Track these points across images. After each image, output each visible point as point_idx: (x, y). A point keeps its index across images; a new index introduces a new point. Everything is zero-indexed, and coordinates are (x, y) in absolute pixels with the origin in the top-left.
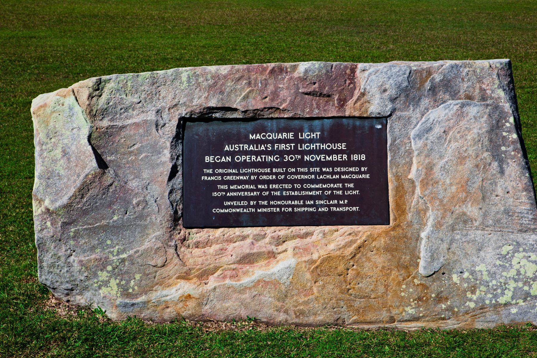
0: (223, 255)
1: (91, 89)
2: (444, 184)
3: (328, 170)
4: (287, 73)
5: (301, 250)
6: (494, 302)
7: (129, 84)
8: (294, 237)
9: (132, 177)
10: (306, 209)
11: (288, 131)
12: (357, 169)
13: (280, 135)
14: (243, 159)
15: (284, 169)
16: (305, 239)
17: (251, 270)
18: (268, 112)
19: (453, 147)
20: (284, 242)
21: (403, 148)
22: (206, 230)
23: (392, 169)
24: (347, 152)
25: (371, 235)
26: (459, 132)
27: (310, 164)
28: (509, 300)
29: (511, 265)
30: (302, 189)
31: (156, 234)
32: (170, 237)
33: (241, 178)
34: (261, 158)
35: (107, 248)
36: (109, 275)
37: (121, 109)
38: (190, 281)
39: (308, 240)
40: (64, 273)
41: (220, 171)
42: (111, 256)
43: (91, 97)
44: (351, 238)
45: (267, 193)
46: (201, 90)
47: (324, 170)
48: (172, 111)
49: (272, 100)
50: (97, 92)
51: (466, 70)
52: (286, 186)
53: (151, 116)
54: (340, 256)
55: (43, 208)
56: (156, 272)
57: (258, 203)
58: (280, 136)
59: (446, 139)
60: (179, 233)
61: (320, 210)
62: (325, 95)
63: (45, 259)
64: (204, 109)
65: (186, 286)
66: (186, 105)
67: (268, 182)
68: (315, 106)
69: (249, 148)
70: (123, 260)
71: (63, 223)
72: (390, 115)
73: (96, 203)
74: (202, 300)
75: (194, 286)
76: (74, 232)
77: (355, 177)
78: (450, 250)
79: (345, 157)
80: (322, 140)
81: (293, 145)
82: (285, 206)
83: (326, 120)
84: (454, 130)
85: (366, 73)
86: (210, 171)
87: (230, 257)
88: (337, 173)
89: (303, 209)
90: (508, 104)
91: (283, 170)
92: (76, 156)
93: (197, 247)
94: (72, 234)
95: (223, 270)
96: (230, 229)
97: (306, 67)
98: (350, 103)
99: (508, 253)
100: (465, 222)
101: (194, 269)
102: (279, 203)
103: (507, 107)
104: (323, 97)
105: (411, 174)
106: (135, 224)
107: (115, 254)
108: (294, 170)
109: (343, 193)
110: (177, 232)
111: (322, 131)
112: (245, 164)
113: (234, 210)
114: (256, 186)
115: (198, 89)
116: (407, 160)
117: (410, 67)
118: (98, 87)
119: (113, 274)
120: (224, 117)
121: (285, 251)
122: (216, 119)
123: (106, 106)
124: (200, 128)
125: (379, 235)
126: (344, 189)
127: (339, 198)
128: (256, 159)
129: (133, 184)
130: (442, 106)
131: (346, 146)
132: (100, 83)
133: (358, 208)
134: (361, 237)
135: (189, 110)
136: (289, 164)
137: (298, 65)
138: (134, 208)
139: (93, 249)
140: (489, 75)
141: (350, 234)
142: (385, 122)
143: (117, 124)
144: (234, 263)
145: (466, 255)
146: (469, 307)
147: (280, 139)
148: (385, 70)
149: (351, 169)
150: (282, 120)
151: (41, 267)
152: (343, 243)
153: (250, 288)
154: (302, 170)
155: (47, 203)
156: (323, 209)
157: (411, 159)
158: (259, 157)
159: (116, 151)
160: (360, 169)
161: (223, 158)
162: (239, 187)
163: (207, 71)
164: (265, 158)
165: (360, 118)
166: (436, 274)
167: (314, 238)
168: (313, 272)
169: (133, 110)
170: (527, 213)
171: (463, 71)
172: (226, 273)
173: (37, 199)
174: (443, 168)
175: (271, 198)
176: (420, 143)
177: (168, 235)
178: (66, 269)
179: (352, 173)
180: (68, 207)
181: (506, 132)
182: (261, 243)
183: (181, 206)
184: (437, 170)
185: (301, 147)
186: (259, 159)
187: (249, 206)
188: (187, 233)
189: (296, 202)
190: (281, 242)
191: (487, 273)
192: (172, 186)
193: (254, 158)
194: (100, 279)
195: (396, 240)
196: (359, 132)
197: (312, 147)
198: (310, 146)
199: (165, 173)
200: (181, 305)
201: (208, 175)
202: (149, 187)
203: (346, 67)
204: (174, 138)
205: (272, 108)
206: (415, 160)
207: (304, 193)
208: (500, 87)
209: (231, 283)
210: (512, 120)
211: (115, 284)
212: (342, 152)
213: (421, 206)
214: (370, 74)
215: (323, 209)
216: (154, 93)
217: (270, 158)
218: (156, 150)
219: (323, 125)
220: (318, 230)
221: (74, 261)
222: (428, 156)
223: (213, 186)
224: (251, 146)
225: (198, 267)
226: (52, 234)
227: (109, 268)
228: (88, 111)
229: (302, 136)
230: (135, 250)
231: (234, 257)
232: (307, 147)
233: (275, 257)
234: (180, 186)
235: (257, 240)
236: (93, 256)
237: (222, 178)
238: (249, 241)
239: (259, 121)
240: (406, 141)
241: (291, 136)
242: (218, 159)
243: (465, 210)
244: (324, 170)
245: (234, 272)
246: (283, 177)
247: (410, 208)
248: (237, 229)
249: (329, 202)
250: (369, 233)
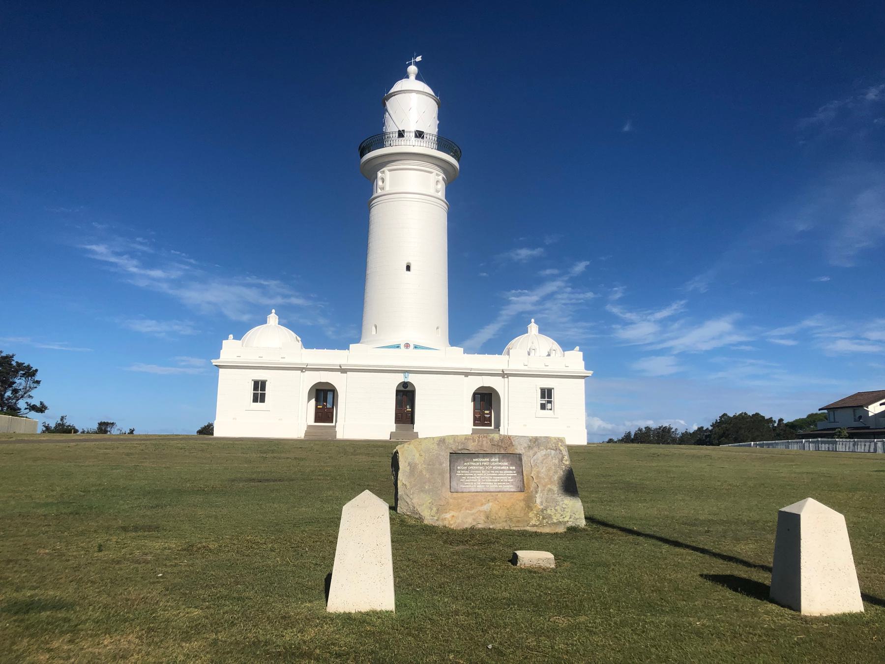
12: (512, 472)
77: (511, 475)
212: (506, 466)
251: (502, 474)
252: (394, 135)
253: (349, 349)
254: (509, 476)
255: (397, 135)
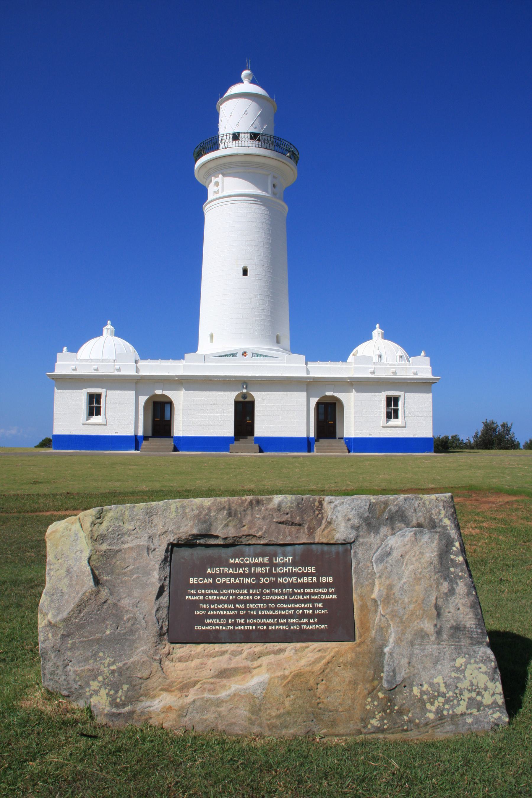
0: (203, 669)
1: (94, 517)
2: (403, 602)
3: (299, 591)
4: (263, 504)
5: (274, 666)
6: (451, 712)
7: (127, 513)
8: (269, 653)
9: (125, 595)
10: (279, 627)
11: (263, 556)
12: (325, 590)
13: (256, 559)
14: (223, 581)
15: (260, 590)
16: (278, 655)
17: (228, 684)
18: (246, 539)
19: (410, 569)
20: (259, 657)
21: (366, 571)
22: (188, 645)
23: (356, 590)
24: (317, 574)
25: (338, 651)
26: (414, 556)
27: (283, 586)
28: (464, 710)
29: (464, 676)
30: (276, 609)
31: (142, 648)
32: (156, 651)
33: (221, 598)
34: (240, 580)
35: (100, 660)
36: (100, 685)
37: (118, 535)
38: (172, 693)
39: (282, 656)
40: (62, 681)
41: (203, 591)
42: (102, 667)
43: (93, 524)
44: (320, 654)
45: (245, 612)
46: (187, 519)
47: (296, 591)
48: (162, 537)
49: (250, 528)
50: (99, 520)
51: (417, 503)
52: (261, 606)
53: (143, 542)
54: (310, 672)
55: (46, 621)
56: (142, 683)
57: (235, 621)
58: (256, 561)
59: (403, 563)
60: (164, 648)
61: (292, 628)
62: (296, 524)
63: (47, 667)
64: (189, 536)
65: (168, 698)
66: (174, 532)
67: (245, 602)
68: (287, 533)
69: (228, 571)
70: (113, 672)
71: (62, 635)
72: (354, 541)
73: (91, 618)
74: (182, 712)
75: (175, 699)
76: (71, 644)
77: (324, 597)
78: (411, 664)
79: (315, 579)
80: (294, 564)
81: (268, 568)
82: (260, 624)
83: (297, 546)
84: (410, 553)
85: (332, 505)
86: (194, 591)
87: (209, 671)
88: (308, 594)
89: (277, 627)
90: (454, 531)
91: (259, 591)
92: (77, 576)
93: (180, 661)
94: (69, 645)
95: (202, 684)
96: (211, 645)
97: (280, 499)
98: (319, 531)
99: (462, 665)
100: (423, 637)
101: (176, 681)
102: (255, 621)
103: (453, 533)
104: (295, 525)
105: (373, 594)
106: (125, 638)
107: (106, 665)
108: (268, 591)
109: (313, 612)
110: (163, 647)
111: (294, 555)
112: (225, 586)
113: (214, 628)
114: (235, 606)
115: (185, 519)
116: (370, 581)
117: (370, 500)
118: (100, 516)
119: (104, 685)
120: (207, 543)
121: (260, 666)
122: (201, 545)
123: (105, 533)
124: (186, 553)
125: (346, 652)
126: (314, 608)
127: (309, 616)
128: (235, 581)
129: (126, 602)
130: (398, 533)
131: (316, 569)
132: (102, 513)
133: (326, 626)
134: (329, 654)
135: (176, 536)
136: (264, 586)
137: (273, 498)
138: (124, 623)
139: (86, 660)
140: (436, 506)
141: (319, 651)
142: (349, 547)
143: (114, 548)
144: (212, 677)
145: (424, 668)
146: (429, 718)
147: (256, 563)
148: (349, 502)
149: (320, 590)
150: (259, 546)
151: (44, 675)
152: (313, 659)
153: (226, 702)
154: (276, 591)
155: (50, 616)
156: (295, 627)
157: (374, 580)
158: (237, 579)
159: (112, 572)
160: (328, 590)
161: (206, 579)
162: (219, 607)
163: (193, 503)
164: (243, 580)
165: (327, 544)
166: (398, 687)
167: (287, 653)
168: (284, 686)
169: (129, 536)
170: (476, 628)
171: (415, 503)
172: (205, 686)
173: (42, 613)
174: (402, 588)
175: (247, 616)
176: (381, 566)
177: (154, 649)
178: (63, 677)
179: (321, 593)
180: (67, 620)
181: (454, 555)
182: (238, 658)
183: (167, 623)
184: (396, 589)
185: (275, 570)
186: (237, 581)
187: (227, 624)
188: (171, 647)
189: (271, 621)
190: (256, 658)
191: (444, 685)
192: (159, 605)
193: (233, 580)
194: (92, 688)
195: (361, 656)
196: (327, 556)
197: (285, 570)
198: (283, 569)
199: (154, 592)
200: (162, 716)
201: (192, 595)
202: (139, 605)
203: (314, 500)
204: (162, 562)
205: (249, 535)
206: (377, 581)
207: (277, 612)
208: (446, 516)
209: (209, 696)
210: (457, 544)
211: (105, 693)
212: (311, 575)
213: (383, 624)
214: (336, 506)
215: (295, 627)
216: (147, 521)
217: (248, 580)
218: (148, 573)
219: (294, 550)
220: (290, 647)
221: (70, 671)
222: (388, 578)
223: (195, 605)
224: (231, 569)
225: (180, 680)
226: (52, 645)
227: (100, 678)
228: (90, 536)
229: (276, 560)
230: (123, 663)
231: (212, 671)
232: (281, 570)
233: (250, 672)
234: (167, 604)
235: (235, 656)
236: (87, 667)
237: (204, 598)
238: (226, 656)
239: (238, 547)
240: (370, 565)
241: (266, 560)
242: (201, 581)
243: (422, 626)
244: (296, 591)
245: (212, 686)
246: (259, 597)
247: (374, 626)
248: (216, 645)
249: (301, 620)
250: (337, 649)
251: (300, 597)
252: (228, 137)
253: (184, 359)
254: (318, 601)
255: (231, 137)
